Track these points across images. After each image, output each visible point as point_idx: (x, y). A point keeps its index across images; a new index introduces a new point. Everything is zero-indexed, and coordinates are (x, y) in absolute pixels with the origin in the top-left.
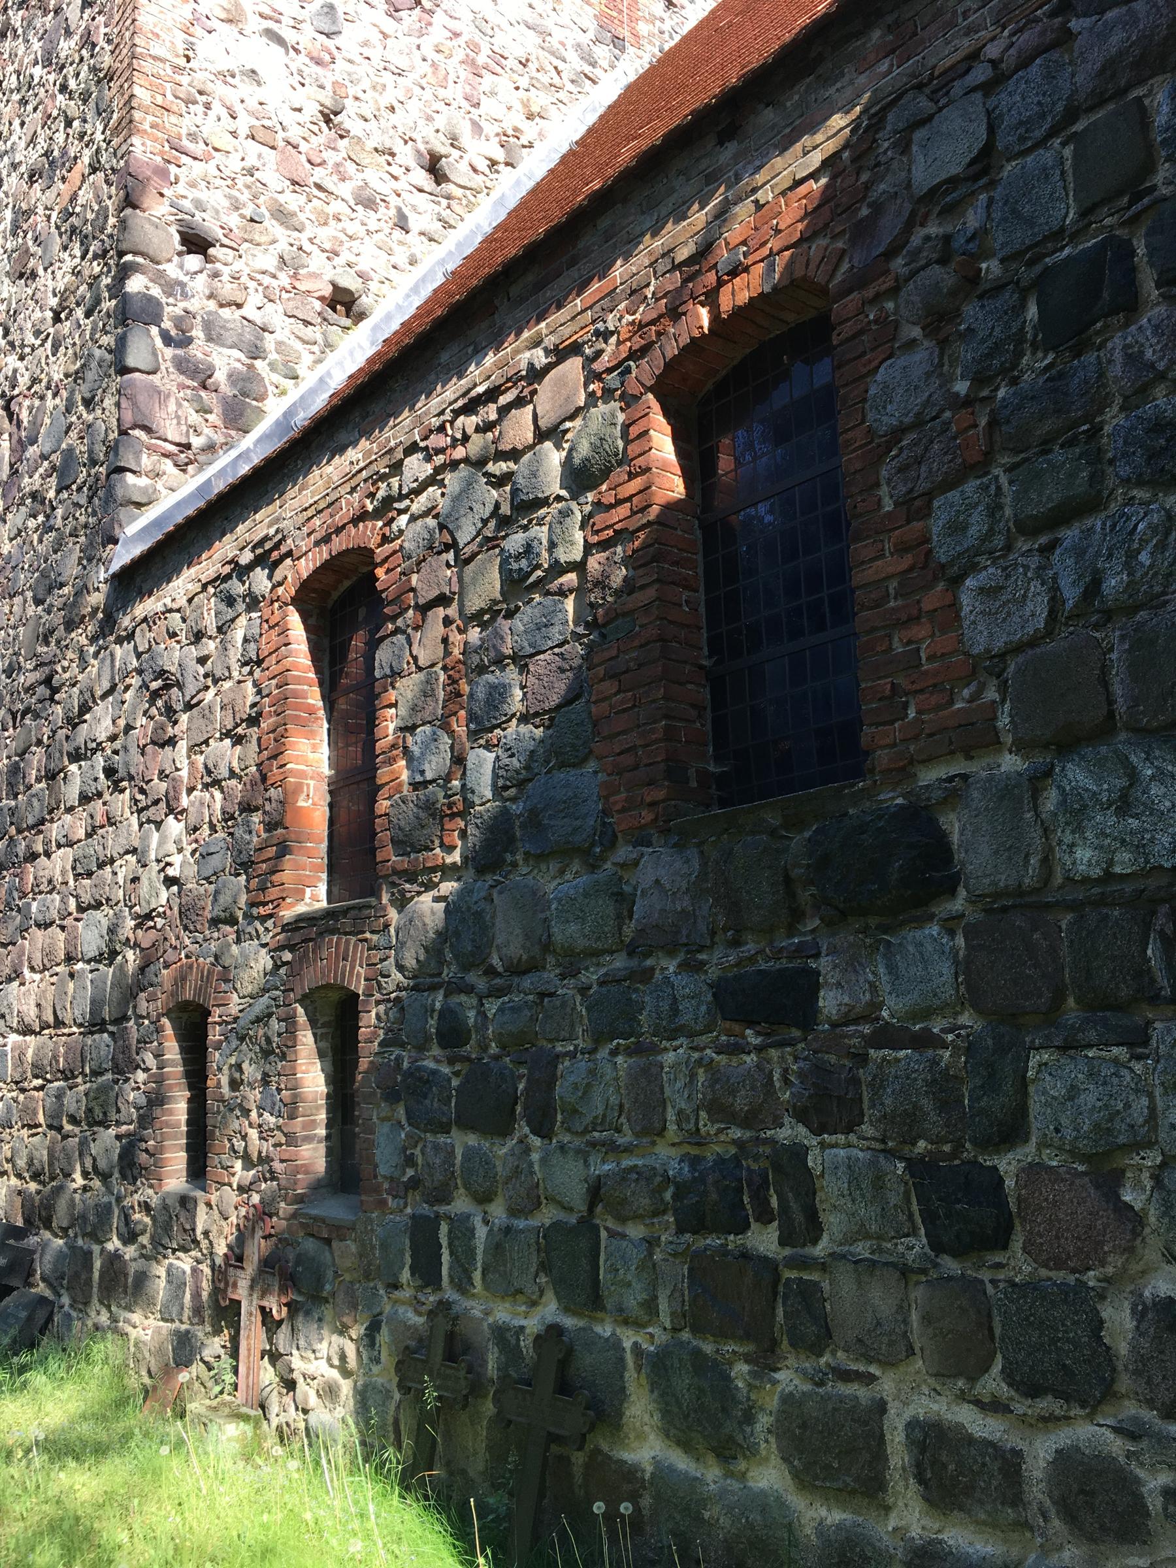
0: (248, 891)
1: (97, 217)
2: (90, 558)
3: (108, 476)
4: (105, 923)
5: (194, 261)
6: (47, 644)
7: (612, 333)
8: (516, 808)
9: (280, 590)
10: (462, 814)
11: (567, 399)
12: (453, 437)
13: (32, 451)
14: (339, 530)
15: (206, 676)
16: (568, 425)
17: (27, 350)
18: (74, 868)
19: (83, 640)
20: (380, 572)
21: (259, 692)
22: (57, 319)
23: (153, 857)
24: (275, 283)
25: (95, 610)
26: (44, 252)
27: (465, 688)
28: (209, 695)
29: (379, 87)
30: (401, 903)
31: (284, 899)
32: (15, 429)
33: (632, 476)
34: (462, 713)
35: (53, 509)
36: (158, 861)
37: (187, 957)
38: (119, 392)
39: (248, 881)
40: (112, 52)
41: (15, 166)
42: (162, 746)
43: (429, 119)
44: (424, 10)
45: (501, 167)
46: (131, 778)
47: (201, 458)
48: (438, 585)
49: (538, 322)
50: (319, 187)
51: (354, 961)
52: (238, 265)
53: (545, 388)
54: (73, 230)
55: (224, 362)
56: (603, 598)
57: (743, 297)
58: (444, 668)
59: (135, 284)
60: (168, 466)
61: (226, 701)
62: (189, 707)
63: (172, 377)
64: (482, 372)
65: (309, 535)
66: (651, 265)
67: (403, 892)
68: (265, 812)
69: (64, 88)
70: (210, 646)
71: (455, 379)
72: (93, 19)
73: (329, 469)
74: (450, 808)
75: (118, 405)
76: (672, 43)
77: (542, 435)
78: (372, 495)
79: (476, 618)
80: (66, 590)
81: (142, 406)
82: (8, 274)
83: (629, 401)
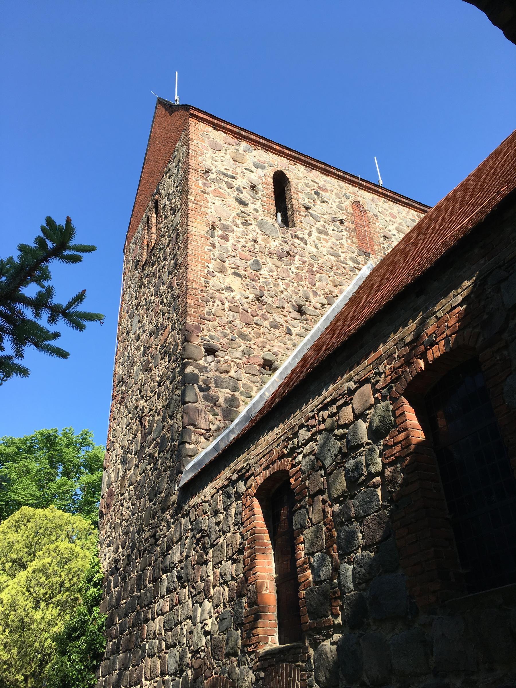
0: (242, 639)
1: (174, 347)
2: (172, 480)
3: (179, 445)
4: (178, 654)
5: (210, 358)
6: (154, 519)
7: (382, 373)
8: (366, 594)
9: (250, 490)
10: (341, 598)
11: (366, 401)
12: (319, 420)
13: (150, 437)
14: (273, 463)
15: (220, 531)
16: (368, 412)
17: (148, 398)
18: (164, 626)
19: (169, 517)
20: (292, 480)
21: (242, 538)
22: (159, 385)
23: (199, 621)
24: (241, 362)
25: (174, 503)
26: (155, 361)
27: (335, 534)
28: (221, 540)
29: (277, 285)
30: (315, 645)
31: (259, 643)
32: (143, 429)
33: (400, 432)
34: (335, 546)
35: (157, 460)
36: (201, 623)
37: (215, 674)
38: (183, 411)
39: (242, 633)
40: (179, 289)
41: (144, 331)
42: (202, 565)
43: (297, 293)
44: (291, 256)
45: (326, 306)
46: (189, 581)
47: (215, 434)
48: (318, 485)
49: (350, 371)
50: (256, 324)
51: (294, 678)
52: (227, 357)
53: (356, 398)
54: (166, 352)
55: (222, 395)
56: (394, 488)
57: (437, 354)
58: (325, 524)
59: (189, 370)
60: (202, 439)
61: (228, 542)
62: (213, 546)
63: (203, 403)
64: (329, 393)
65: (261, 466)
66: (395, 345)
67: (315, 639)
68: (248, 597)
69: (162, 303)
70: (221, 517)
71: (317, 397)
72: (172, 278)
73: (267, 437)
74: (334, 594)
75: (182, 417)
76: (389, 251)
77: (357, 417)
78: (286, 447)
79: (337, 500)
80: (162, 495)
81: (192, 416)
82: (141, 370)
83: (394, 400)
